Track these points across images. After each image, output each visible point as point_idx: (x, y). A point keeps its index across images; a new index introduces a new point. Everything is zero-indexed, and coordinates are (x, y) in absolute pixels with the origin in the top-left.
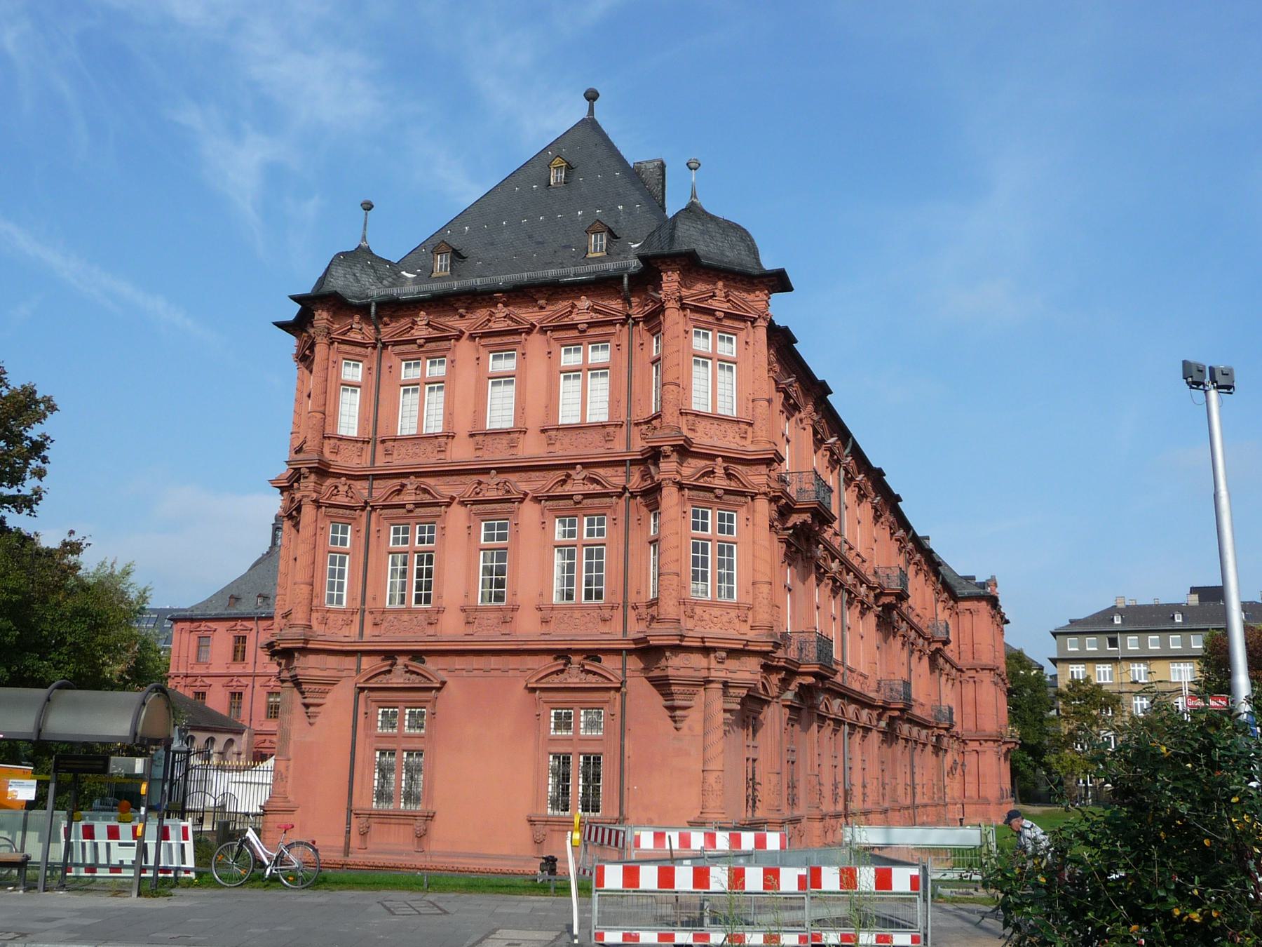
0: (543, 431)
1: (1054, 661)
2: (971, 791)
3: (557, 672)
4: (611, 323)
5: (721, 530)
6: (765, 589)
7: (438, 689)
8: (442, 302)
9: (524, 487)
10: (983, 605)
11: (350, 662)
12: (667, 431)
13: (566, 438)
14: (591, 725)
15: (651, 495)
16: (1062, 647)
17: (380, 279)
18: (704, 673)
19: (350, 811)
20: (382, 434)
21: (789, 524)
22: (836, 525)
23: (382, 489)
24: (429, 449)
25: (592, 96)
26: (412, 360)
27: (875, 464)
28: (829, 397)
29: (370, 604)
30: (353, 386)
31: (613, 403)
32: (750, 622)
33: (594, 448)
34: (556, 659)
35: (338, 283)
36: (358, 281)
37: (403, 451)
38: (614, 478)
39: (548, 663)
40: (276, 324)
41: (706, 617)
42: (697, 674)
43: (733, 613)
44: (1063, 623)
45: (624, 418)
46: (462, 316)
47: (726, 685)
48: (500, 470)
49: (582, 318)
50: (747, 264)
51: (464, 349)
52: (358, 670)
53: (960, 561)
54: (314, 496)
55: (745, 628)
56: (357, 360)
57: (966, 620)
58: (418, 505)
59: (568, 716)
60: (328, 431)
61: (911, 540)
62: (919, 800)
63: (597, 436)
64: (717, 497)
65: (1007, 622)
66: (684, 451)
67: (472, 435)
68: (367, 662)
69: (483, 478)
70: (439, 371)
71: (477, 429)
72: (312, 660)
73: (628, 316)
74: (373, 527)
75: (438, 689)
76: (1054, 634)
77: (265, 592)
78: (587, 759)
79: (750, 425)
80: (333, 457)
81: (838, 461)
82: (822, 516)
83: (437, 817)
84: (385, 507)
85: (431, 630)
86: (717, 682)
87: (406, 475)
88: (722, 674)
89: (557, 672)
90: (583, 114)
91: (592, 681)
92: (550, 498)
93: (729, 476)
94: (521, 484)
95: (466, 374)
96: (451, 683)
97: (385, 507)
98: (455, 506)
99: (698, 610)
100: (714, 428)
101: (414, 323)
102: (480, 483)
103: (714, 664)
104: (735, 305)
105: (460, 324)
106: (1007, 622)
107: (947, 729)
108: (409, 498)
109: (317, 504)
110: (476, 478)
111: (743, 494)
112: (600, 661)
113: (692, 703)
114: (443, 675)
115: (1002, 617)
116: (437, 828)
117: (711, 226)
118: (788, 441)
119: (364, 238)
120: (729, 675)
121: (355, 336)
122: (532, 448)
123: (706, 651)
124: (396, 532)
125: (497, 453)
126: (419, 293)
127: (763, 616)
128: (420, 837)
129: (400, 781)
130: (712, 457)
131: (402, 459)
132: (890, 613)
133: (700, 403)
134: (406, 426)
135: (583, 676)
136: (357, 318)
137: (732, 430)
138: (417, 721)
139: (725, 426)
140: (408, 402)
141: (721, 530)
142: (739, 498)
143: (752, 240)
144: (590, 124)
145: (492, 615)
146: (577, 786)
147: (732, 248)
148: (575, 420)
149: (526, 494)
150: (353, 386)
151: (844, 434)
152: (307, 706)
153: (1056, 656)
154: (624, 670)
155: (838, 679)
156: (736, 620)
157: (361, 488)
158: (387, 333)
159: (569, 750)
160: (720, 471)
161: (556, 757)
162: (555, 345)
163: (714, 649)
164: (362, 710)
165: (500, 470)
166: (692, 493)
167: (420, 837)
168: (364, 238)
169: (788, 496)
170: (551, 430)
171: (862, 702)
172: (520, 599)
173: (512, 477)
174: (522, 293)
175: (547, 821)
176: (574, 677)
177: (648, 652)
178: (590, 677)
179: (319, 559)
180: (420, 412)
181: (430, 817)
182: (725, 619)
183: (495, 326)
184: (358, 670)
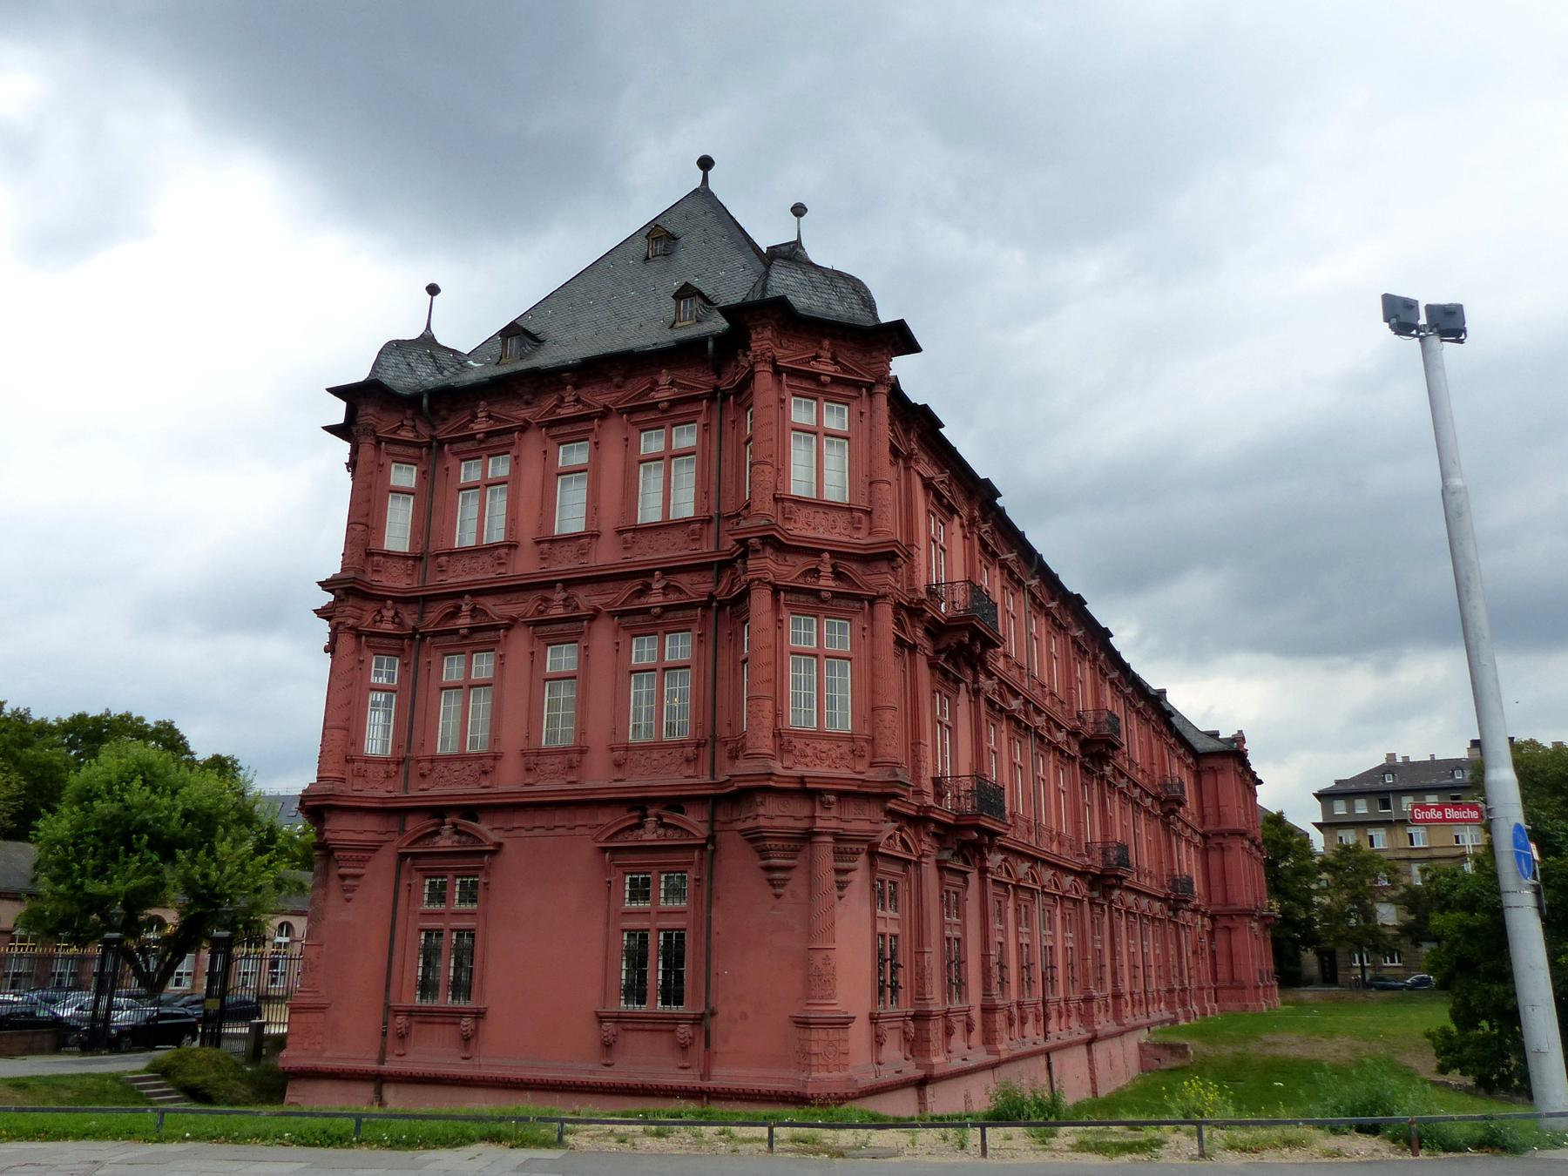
7: (492, 853)
9: (597, 601)
10: (1231, 764)
14: (674, 892)
16: (1327, 810)
19: (388, 1007)
21: (942, 646)
22: (1125, 748)
25: (706, 163)
28: (999, 501)
31: (702, 493)
34: (630, 811)
35: (388, 378)
37: (460, 566)
39: (624, 818)
40: (326, 428)
41: (809, 751)
44: (1328, 784)
46: (528, 403)
47: (838, 837)
48: (568, 583)
49: (663, 395)
50: (860, 317)
59: (646, 882)
60: (373, 547)
63: (678, 536)
65: (1260, 782)
66: (781, 547)
69: (548, 594)
73: (716, 388)
75: (492, 853)
83: (488, 1014)
84: (435, 634)
87: (460, 595)
88: (833, 824)
89: (631, 828)
90: (697, 183)
91: (673, 838)
92: (622, 614)
93: (838, 575)
100: (819, 517)
104: (845, 369)
105: (526, 413)
106: (1260, 782)
110: (540, 593)
112: (682, 812)
113: (851, 865)
116: (489, 1028)
117: (815, 276)
122: (606, 555)
125: (565, 563)
130: (817, 553)
131: (458, 576)
133: (800, 483)
134: (465, 537)
135: (661, 831)
138: (469, 894)
139: (833, 515)
140: (467, 509)
142: (688, 612)
143: (867, 291)
144: (703, 193)
146: (656, 973)
147: (841, 299)
149: (597, 611)
153: (1320, 820)
158: (442, 432)
159: (646, 925)
160: (826, 569)
163: (820, 792)
170: (633, 532)
175: (619, 1018)
181: (479, 1015)
183: (566, 412)
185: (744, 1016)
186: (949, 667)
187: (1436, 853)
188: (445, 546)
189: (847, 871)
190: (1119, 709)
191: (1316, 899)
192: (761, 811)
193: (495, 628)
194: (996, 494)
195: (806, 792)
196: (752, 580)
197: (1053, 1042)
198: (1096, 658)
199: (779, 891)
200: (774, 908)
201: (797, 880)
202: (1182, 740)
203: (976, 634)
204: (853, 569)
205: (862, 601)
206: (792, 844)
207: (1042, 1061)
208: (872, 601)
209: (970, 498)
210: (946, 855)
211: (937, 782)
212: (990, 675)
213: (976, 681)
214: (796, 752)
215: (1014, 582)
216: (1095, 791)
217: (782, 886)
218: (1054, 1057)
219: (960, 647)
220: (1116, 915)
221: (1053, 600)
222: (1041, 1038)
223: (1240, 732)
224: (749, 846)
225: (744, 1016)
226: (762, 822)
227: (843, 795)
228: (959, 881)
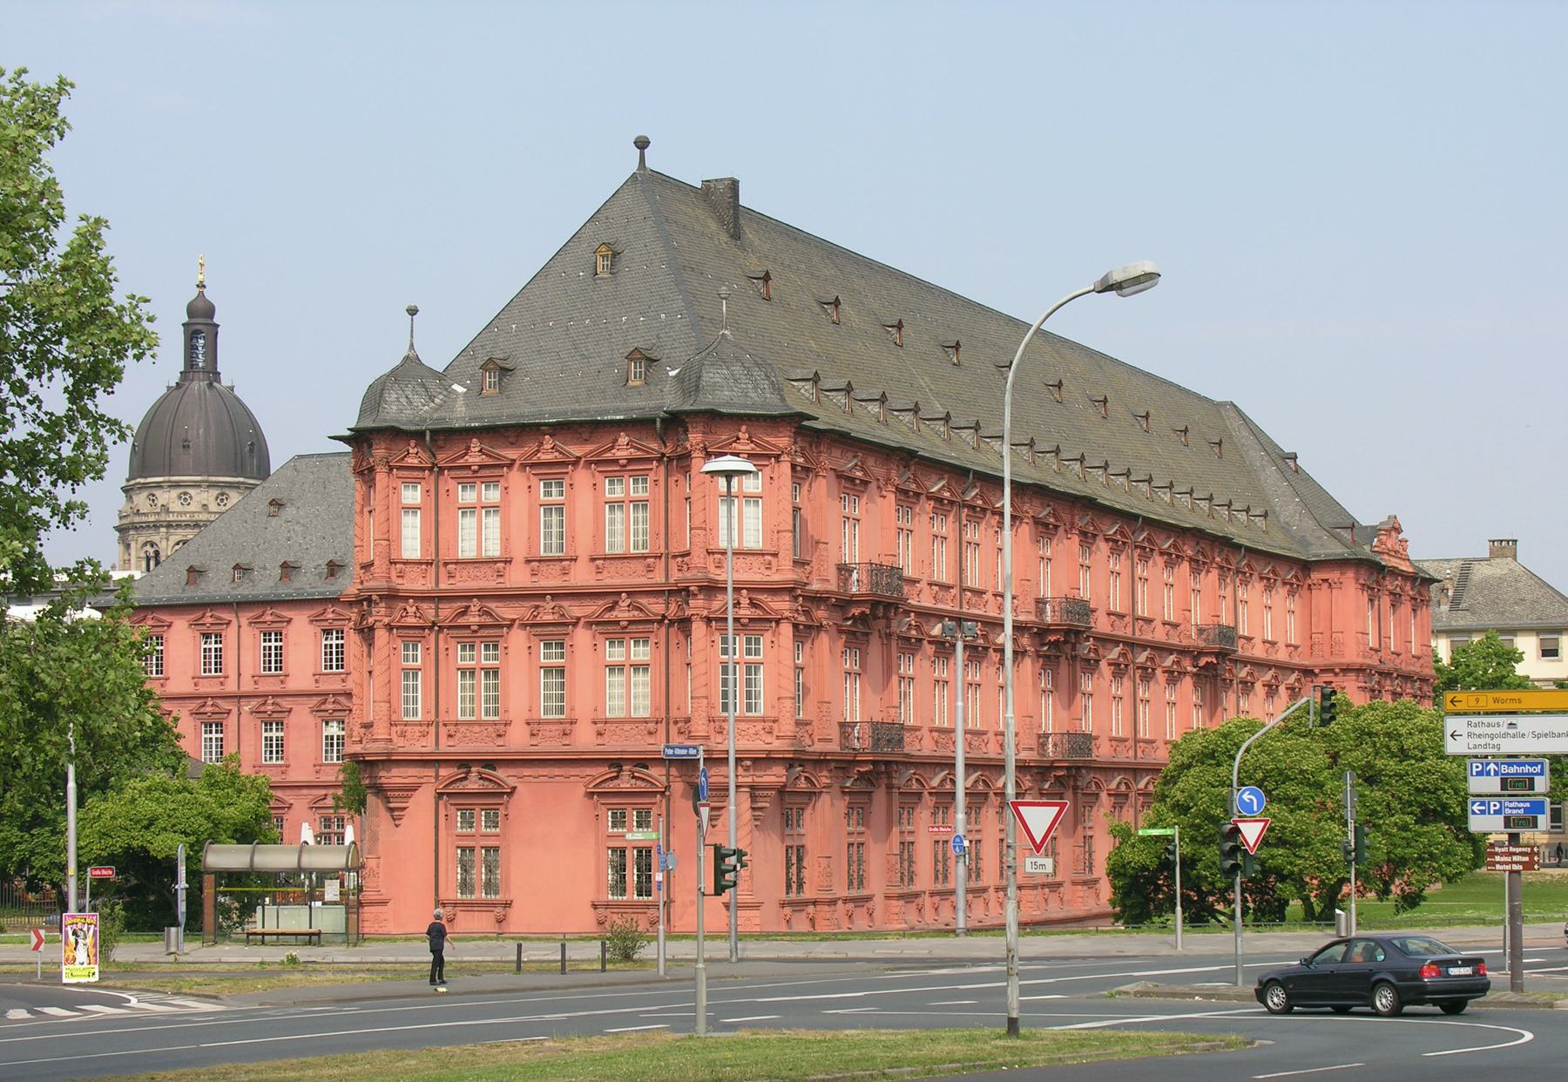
0: (593, 560)
3: (611, 779)
4: (650, 460)
5: (749, 652)
8: (492, 432)
11: (430, 772)
12: (695, 571)
13: (612, 567)
15: (684, 624)
17: (432, 398)
20: (444, 556)
23: (447, 611)
24: (489, 572)
25: (642, 144)
26: (468, 483)
29: (443, 717)
30: (413, 509)
32: (776, 733)
33: (634, 577)
36: (410, 402)
37: (465, 573)
38: (656, 607)
43: (760, 726)
45: (662, 550)
48: (555, 596)
51: (516, 478)
52: (437, 777)
54: (386, 620)
55: (769, 739)
56: (414, 482)
58: (481, 627)
67: (528, 561)
68: (444, 772)
70: (493, 495)
71: (532, 556)
72: (395, 771)
74: (442, 646)
77: (243, 561)
78: (640, 852)
79: (775, 555)
80: (400, 581)
84: (449, 628)
85: (500, 741)
88: (749, 780)
89: (611, 779)
92: (598, 623)
93: (753, 604)
94: (575, 609)
95: (519, 501)
96: (521, 788)
97: (449, 628)
98: (515, 630)
101: (468, 448)
102: (537, 607)
105: (511, 454)
108: (473, 619)
109: (389, 627)
111: (769, 620)
114: (512, 782)
116: (513, 913)
119: (412, 345)
121: (412, 461)
124: (463, 648)
125: (550, 580)
126: (471, 420)
128: (500, 922)
129: (480, 874)
131: (465, 582)
134: (467, 550)
136: (413, 443)
137: (756, 562)
140: (467, 524)
141: (749, 652)
145: (554, 727)
148: (619, 551)
150: (413, 509)
152: (392, 810)
154: (668, 775)
157: (429, 610)
158: (442, 458)
161: (614, 850)
162: (600, 477)
164: (442, 813)
165: (555, 596)
167: (500, 922)
168: (412, 345)
172: (577, 714)
173: (565, 604)
174: (565, 429)
176: (625, 783)
177: (687, 764)
178: (639, 783)
179: (394, 677)
180: (479, 536)
181: (507, 905)
182: (752, 731)
183: (544, 457)
184: (437, 777)
188: (451, 557)
193: (501, 626)
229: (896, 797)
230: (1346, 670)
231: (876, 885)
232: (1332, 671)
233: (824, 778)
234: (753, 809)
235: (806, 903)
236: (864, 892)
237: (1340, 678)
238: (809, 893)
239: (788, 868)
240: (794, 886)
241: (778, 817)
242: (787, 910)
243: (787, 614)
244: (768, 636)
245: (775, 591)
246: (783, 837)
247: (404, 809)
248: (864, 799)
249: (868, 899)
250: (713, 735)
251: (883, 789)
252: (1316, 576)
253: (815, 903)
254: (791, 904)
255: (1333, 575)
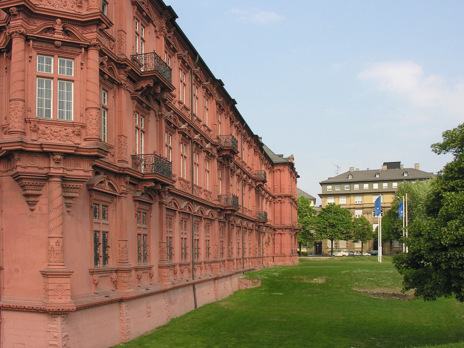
1: (321, 196)
2: (277, 251)
6: (94, 112)
18: (45, 171)
21: (139, 88)
22: (239, 155)
27: (217, 77)
32: (84, 136)
41: (48, 132)
42: (41, 171)
43: (70, 130)
44: (325, 179)
47: (64, 179)
53: (275, 146)
57: (277, 174)
61: (244, 128)
62: (247, 255)
64: (57, 47)
65: (298, 177)
76: (322, 184)
81: (223, 110)
82: (234, 152)
86: (56, 177)
88: (61, 171)
93: (66, 32)
99: (42, 127)
103: (52, 164)
106: (298, 177)
107: (264, 223)
113: (41, 192)
115: (296, 173)
118: (207, 109)
120: (66, 172)
123: (47, 155)
127: (92, 131)
132: (258, 186)
142: (75, 49)
151: (242, 121)
155: (240, 211)
156: (72, 135)
160: (59, 28)
163: (52, 153)
166: (36, 44)
169: (221, 145)
171: (249, 220)
182: (63, 133)
185: (17, 270)
186: (143, 100)
187: (365, 206)
189: (72, 198)
190: (239, 138)
191: (403, 196)
192: (18, 163)
194: (175, 16)
195: (46, 154)
196: (12, 33)
197: (196, 280)
198: (228, 113)
199: (32, 207)
200: (30, 216)
201: (42, 201)
202: (266, 155)
203: (158, 82)
204: (77, 30)
205: (81, 48)
206: (39, 183)
207: (192, 286)
208: (87, 48)
209: (160, 15)
210: (138, 194)
211: (134, 157)
212: (169, 109)
213: (160, 110)
214: (40, 132)
215: (185, 67)
216: (225, 173)
217: (34, 205)
218: (196, 286)
219: (151, 93)
220: (231, 227)
221: (207, 81)
222: (191, 278)
223: (292, 155)
224: (16, 183)
225: (17, 270)
226: (19, 169)
227: (66, 156)
228: (223, 225)
229: (165, 212)
230: (286, 196)
231: (154, 261)
232: (281, 197)
233: (121, 186)
234: (66, 197)
235: (111, 271)
236: (148, 264)
237: (283, 199)
238: (112, 264)
239: (96, 250)
240: (101, 259)
241: (88, 208)
242: (96, 277)
243: (94, 42)
244: (79, 59)
245: (85, 24)
246: (92, 223)
247: (37, 202)
248: (146, 207)
249: (150, 268)
250: (28, 132)
251: (157, 203)
252: (276, 168)
253: (117, 271)
254: (98, 272)
255: (281, 168)
